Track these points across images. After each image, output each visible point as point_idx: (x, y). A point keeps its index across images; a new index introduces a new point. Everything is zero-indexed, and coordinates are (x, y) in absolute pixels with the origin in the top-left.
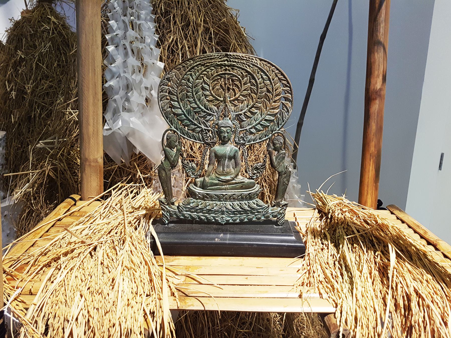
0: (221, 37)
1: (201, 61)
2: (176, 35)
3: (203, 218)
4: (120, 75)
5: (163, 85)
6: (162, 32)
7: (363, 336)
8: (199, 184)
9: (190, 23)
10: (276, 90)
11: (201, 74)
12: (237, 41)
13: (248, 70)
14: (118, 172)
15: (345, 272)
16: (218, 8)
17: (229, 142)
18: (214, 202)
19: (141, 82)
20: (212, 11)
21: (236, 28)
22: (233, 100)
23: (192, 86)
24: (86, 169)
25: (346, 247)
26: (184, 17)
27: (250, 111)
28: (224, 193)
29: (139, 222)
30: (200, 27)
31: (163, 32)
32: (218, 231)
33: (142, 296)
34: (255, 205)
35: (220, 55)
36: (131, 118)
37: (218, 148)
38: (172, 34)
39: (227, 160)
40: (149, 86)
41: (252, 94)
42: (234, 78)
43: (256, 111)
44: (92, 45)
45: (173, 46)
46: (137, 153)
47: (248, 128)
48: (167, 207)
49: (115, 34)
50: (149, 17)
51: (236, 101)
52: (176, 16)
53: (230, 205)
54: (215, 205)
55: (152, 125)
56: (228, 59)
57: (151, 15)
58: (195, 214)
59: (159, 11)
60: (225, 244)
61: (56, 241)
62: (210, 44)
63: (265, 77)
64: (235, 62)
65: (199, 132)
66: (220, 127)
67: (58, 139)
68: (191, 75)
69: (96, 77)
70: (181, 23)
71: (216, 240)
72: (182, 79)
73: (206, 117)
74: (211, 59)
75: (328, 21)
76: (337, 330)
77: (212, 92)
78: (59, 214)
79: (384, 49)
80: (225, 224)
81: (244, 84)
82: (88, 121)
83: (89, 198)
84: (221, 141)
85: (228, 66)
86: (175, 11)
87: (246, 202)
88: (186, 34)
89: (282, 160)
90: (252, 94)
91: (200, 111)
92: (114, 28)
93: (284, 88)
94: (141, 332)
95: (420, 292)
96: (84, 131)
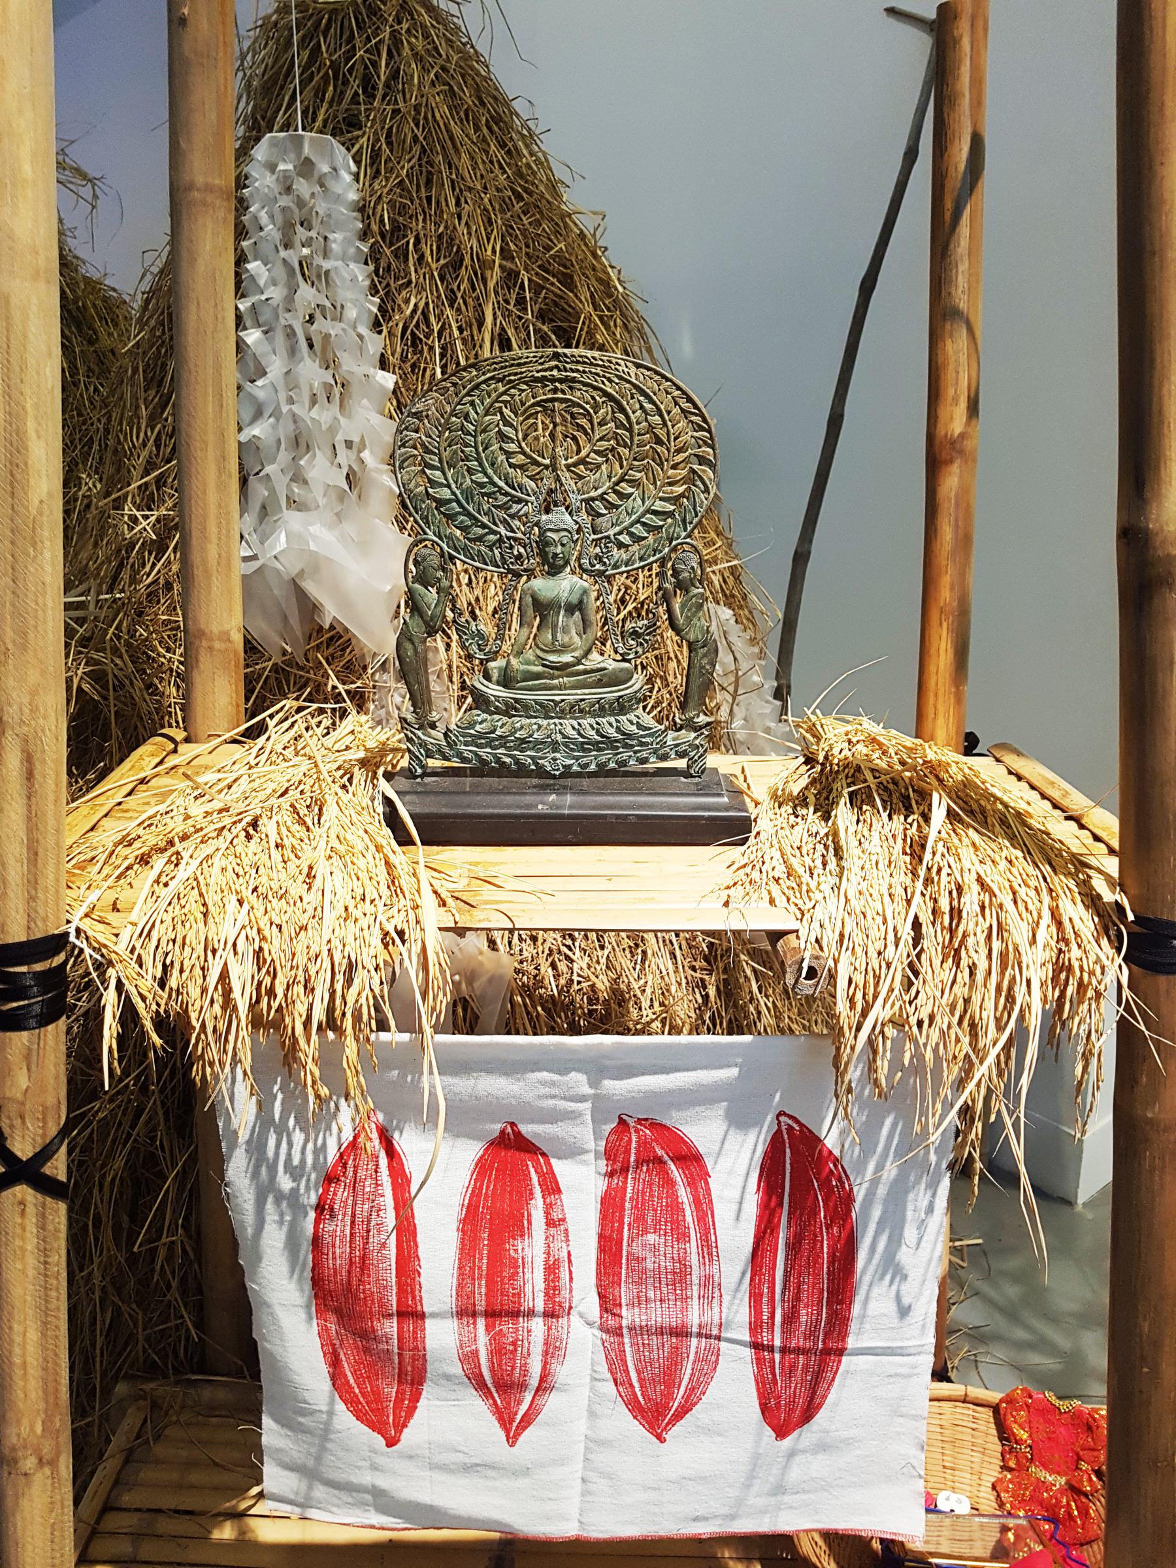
0: (551, 296)
1: (495, 369)
2: (424, 294)
3: (507, 760)
4: (278, 407)
5: (406, 429)
6: (383, 285)
7: (855, 969)
8: (495, 675)
9: (462, 260)
10: (675, 439)
11: (496, 401)
12: (596, 307)
13: (609, 390)
14: (272, 682)
15: (833, 859)
16: (541, 212)
17: (568, 569)
18: (534, 721)
19: (333, 429)
20: (526, 222)
21: (594, 269)
22: (575, 465)
23: (475, 431)
24: (201, 659)
25: (843, 814)
26: (447, 242)
27: (615, 492)
28: (558, 698)
29: (352, 777)
30: (492, 269)
31: (388, 285)
32: (544, 789)
33: (377, 902)
34: (634, 728)
35: (539, 355)
36: (311, 524)
37: (542, 586)
38: (414, 292)
39: (562, 613)
40: (356, 439)
41: (620, 449)
42: (575, 410)
43: (631, 490)
44: (215, 330)
45: (417, 326)
46: (327, 626)
47: (611, 533)
48: (419, 733)
49: (263, 298)
50: (352, 250)
51: (582, 467)
52: (423, 241)
53: (574, 728)
54: (535, 727)
55: (363, 546)
56: (560, 365)
57: (358, 244)
58: (489, 750)
59: (375, 228)
60: (562, 816)
61: (150, 818)
62: (520, 318)
63: (648, 406)
64: (578, 371)
65: (494, 544)
66: (545, 531)
67: (99, 593)
68: (472, 403)
69: (224, 415)
70: (438, 260)
71: (540, 807)
72: (451, 415)
73: (511, 507)
74: (519, 365)
75: (881, 237)
76: (798, 957)
77: (523, 444)
78: (142, 769)
79: (970, 330)
80: (562, 776)
81: (600, 424)
82: (204, 530)
83: (209, 736)
84: (546, 568)
85: (561, 381)
86: (421, 224)
87: (612, 720)
88: (452, 291)
89: (696, 612)
90: (620, 449)
91: (494, 493)
92: (262, 283)
93: (695, 434)
94: (377, 966)
95: (988, 880)
96: (196, 558)
